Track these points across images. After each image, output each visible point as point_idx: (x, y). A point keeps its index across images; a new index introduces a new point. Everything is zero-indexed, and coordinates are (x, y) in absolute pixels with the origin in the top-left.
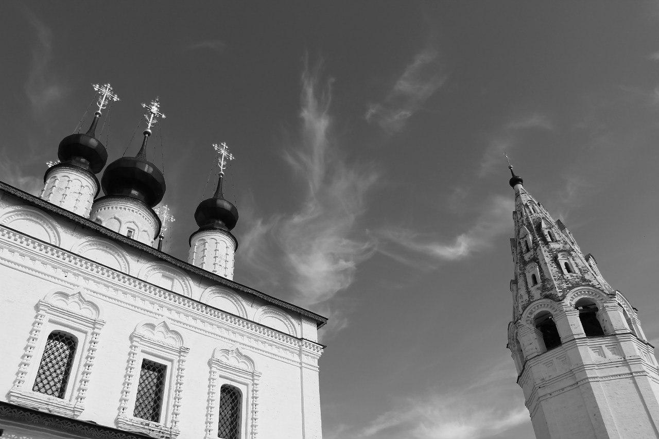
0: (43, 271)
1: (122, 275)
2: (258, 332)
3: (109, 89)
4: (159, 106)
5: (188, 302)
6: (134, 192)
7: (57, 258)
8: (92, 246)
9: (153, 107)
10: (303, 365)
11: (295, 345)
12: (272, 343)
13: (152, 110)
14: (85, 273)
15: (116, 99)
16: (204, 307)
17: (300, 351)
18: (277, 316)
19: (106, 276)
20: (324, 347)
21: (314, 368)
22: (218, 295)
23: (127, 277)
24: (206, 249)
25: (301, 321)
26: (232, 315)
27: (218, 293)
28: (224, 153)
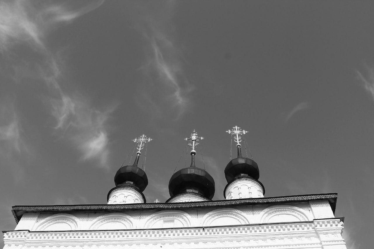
0: (284, 244)
1: (124, 232)
2: (263, 230)
3: (238, 129)
4: (197, 134)
5: (277, 227)
6: (242, 175)
7: (75, 239)
8: (272, 214)
9: (192, 137)
10: (323, 243)
11: (306, 228)
12: (282, 236)
13: (192, 139)
14: (96, 241)
15: (244, 132)
16: (201, 230)
17: (316, 232)
18: (283, 212)
19: (291, 229)
20: (342, 220)
21: (340, 243)
22: (217, 217)
23: (128, 232)
24: (232, 192)
25: (310, 207)
26: (172, 228)
27: (217, 215)
28: (237, 132)
